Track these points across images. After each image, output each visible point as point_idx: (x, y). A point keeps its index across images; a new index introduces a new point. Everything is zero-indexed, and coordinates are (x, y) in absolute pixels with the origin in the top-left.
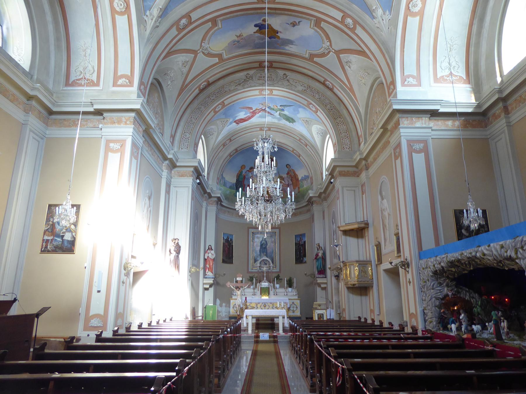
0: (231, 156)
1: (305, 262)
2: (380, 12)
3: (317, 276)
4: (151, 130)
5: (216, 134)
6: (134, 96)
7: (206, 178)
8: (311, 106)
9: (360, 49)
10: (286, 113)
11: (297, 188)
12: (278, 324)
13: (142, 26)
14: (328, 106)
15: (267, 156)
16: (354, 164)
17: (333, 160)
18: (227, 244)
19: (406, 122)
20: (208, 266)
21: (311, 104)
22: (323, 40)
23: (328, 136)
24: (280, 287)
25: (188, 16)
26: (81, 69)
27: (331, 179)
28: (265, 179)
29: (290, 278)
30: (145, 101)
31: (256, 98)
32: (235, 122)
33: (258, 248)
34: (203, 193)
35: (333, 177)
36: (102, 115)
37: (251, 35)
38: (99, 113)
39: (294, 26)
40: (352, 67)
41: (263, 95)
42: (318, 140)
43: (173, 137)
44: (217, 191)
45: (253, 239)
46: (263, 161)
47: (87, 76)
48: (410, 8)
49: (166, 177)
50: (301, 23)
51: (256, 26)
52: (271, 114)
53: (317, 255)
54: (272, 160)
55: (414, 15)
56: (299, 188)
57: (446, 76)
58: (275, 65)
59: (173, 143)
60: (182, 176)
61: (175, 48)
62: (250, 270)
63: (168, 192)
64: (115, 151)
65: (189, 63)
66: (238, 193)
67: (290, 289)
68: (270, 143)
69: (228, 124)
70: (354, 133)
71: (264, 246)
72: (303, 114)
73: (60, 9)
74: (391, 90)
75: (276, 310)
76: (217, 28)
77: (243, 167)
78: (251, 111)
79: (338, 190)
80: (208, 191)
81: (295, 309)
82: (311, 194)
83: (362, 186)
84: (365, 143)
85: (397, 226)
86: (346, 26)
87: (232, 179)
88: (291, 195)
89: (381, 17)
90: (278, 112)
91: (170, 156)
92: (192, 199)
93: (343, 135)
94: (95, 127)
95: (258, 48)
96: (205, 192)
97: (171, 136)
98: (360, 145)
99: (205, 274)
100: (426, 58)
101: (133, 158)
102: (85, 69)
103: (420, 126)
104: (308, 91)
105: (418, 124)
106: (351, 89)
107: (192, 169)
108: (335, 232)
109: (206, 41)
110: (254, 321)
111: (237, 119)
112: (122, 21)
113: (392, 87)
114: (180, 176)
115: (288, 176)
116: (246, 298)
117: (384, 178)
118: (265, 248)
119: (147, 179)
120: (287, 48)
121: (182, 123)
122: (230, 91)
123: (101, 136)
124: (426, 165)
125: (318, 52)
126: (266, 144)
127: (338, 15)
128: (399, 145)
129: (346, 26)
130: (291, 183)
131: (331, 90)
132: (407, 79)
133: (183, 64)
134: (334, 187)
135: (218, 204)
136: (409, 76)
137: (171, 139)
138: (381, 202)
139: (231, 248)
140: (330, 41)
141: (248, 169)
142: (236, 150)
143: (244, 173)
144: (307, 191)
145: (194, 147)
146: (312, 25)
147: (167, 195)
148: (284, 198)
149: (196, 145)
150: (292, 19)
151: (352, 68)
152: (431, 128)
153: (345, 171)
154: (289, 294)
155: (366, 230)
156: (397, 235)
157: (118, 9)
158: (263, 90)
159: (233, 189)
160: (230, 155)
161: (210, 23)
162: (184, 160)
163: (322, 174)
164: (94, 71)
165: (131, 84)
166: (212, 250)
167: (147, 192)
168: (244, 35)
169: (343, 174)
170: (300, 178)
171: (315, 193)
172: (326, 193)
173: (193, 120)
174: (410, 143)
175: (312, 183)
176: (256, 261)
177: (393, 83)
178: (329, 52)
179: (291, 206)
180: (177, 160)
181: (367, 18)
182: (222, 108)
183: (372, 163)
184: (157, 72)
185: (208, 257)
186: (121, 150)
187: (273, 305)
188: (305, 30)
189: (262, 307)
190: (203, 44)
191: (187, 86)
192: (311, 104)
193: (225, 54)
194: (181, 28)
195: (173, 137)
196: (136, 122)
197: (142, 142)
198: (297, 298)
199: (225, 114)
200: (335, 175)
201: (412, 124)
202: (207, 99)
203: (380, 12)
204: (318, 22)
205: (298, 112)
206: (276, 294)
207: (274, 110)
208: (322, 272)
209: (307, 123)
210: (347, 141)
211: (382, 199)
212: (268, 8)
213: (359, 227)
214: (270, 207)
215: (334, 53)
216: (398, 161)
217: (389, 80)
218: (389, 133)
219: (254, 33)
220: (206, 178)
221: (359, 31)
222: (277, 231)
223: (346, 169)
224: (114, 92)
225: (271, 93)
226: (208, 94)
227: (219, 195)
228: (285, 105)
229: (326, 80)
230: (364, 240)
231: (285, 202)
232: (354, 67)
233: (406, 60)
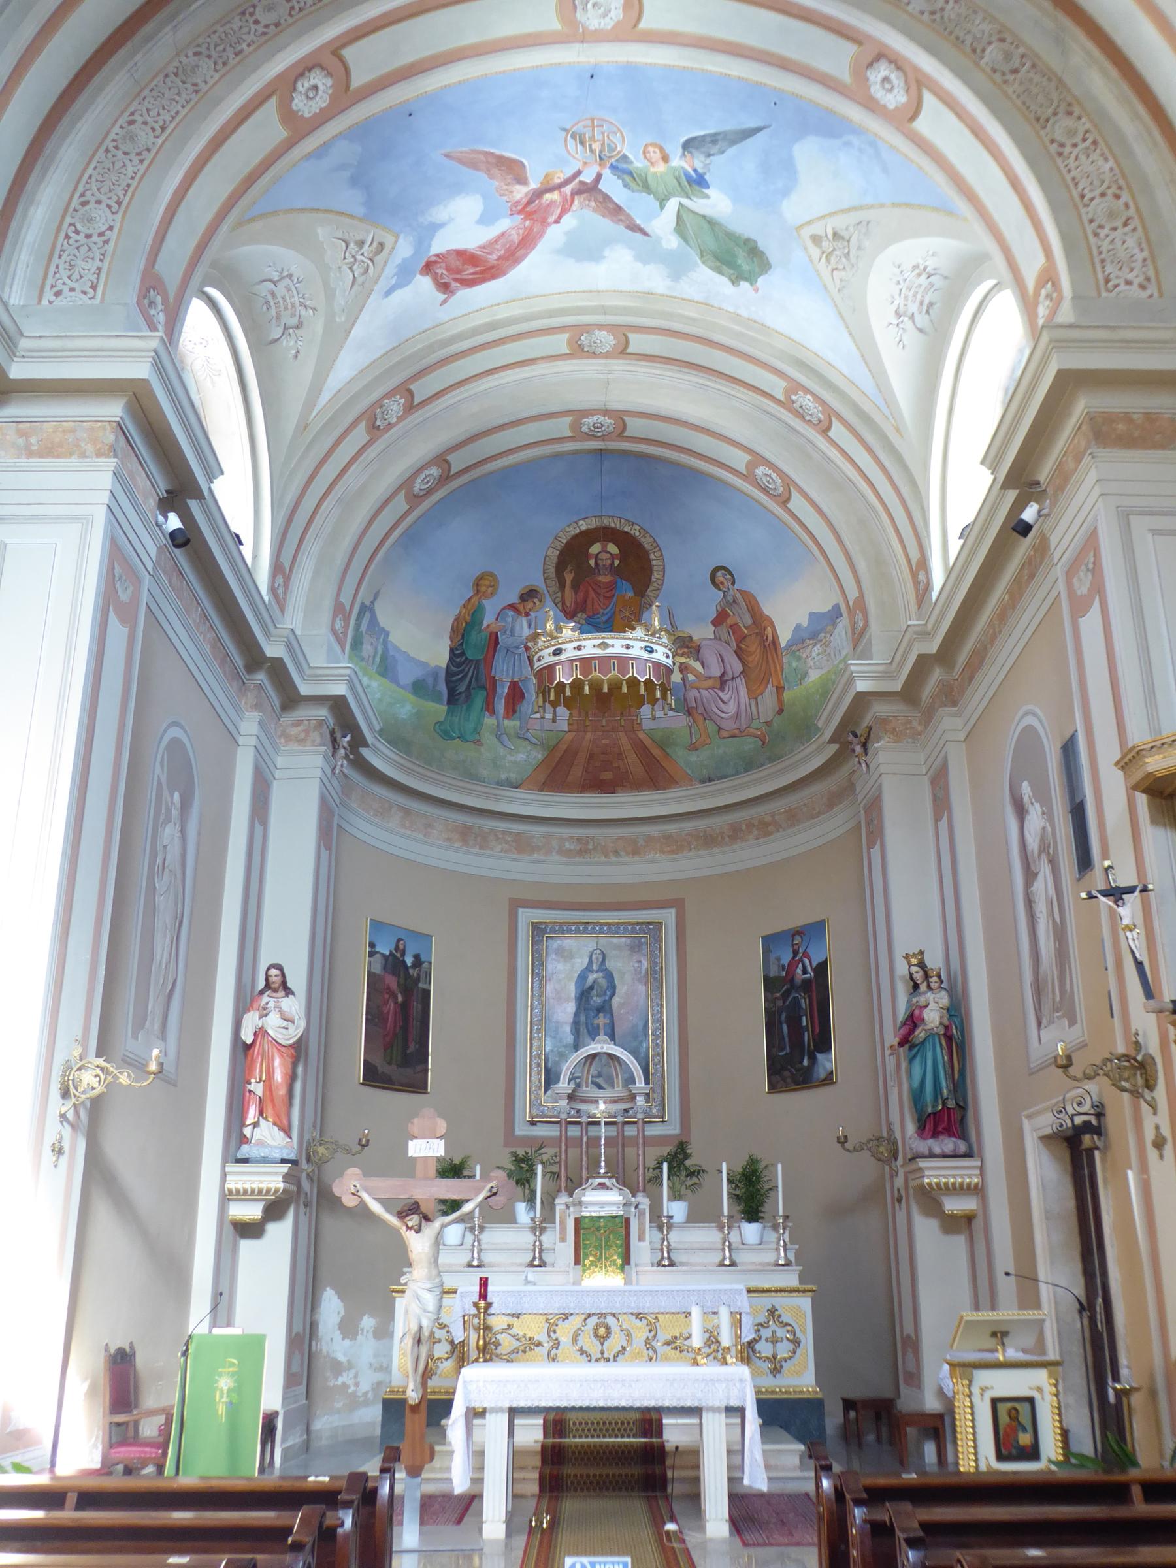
0: (415, 499)
1: (828, 1080)
3: (923, 1146)
5: (317, 326)
10: (716, 203)
11: (769, 693)
12: (693, 1457)
14: (993, 53)
18: (392, 981)
20: (257, 1088)
21: (882, 55)
24: (694, 1218)
27: (1019, 505)
29: (753, 1161)
32: (428, 267)
33: (566, 1011)
34: (239, 662)
45: (539, 962)
52: (635, 228)
53: (913, 1021)
56: (780, 690)
60: (49, 450)
67: (751, 1231)
71: (596, 1000)
75: (683, 1370)
77: (484, 584)
78: (520, 192)
79: (1091, 542)
80: (272, 650)
81: (783, 1350)
93: (1099, 207)
96: (254, 659)
99: (235, 1135)
107: (115, 409)
110: (531, 1434)
114: (31, 454)
115: (723, 631)
116: (484, 1283)
118: (605, 1008)
130: (737, 667)
134: (1043, 548)
139: (416, 1006)
141: (514, 599)
143: (488, 619)
153: (1127, 418)
154: (742, 1257)
159: (436, 698)
166: (289, 992)
169: (1107, 433)
170: (784, 637)
173: (144, 137)
176: (551, 1077)
185: (260, 1033)
187: (652, 1329)
189: (588, 1342)
198: (791, 1279)
202: (236, 23)
206: (667, 1261)
207: (646, 187)
208: (947, 1118)
227: (340, 690)
228: (714, 139)
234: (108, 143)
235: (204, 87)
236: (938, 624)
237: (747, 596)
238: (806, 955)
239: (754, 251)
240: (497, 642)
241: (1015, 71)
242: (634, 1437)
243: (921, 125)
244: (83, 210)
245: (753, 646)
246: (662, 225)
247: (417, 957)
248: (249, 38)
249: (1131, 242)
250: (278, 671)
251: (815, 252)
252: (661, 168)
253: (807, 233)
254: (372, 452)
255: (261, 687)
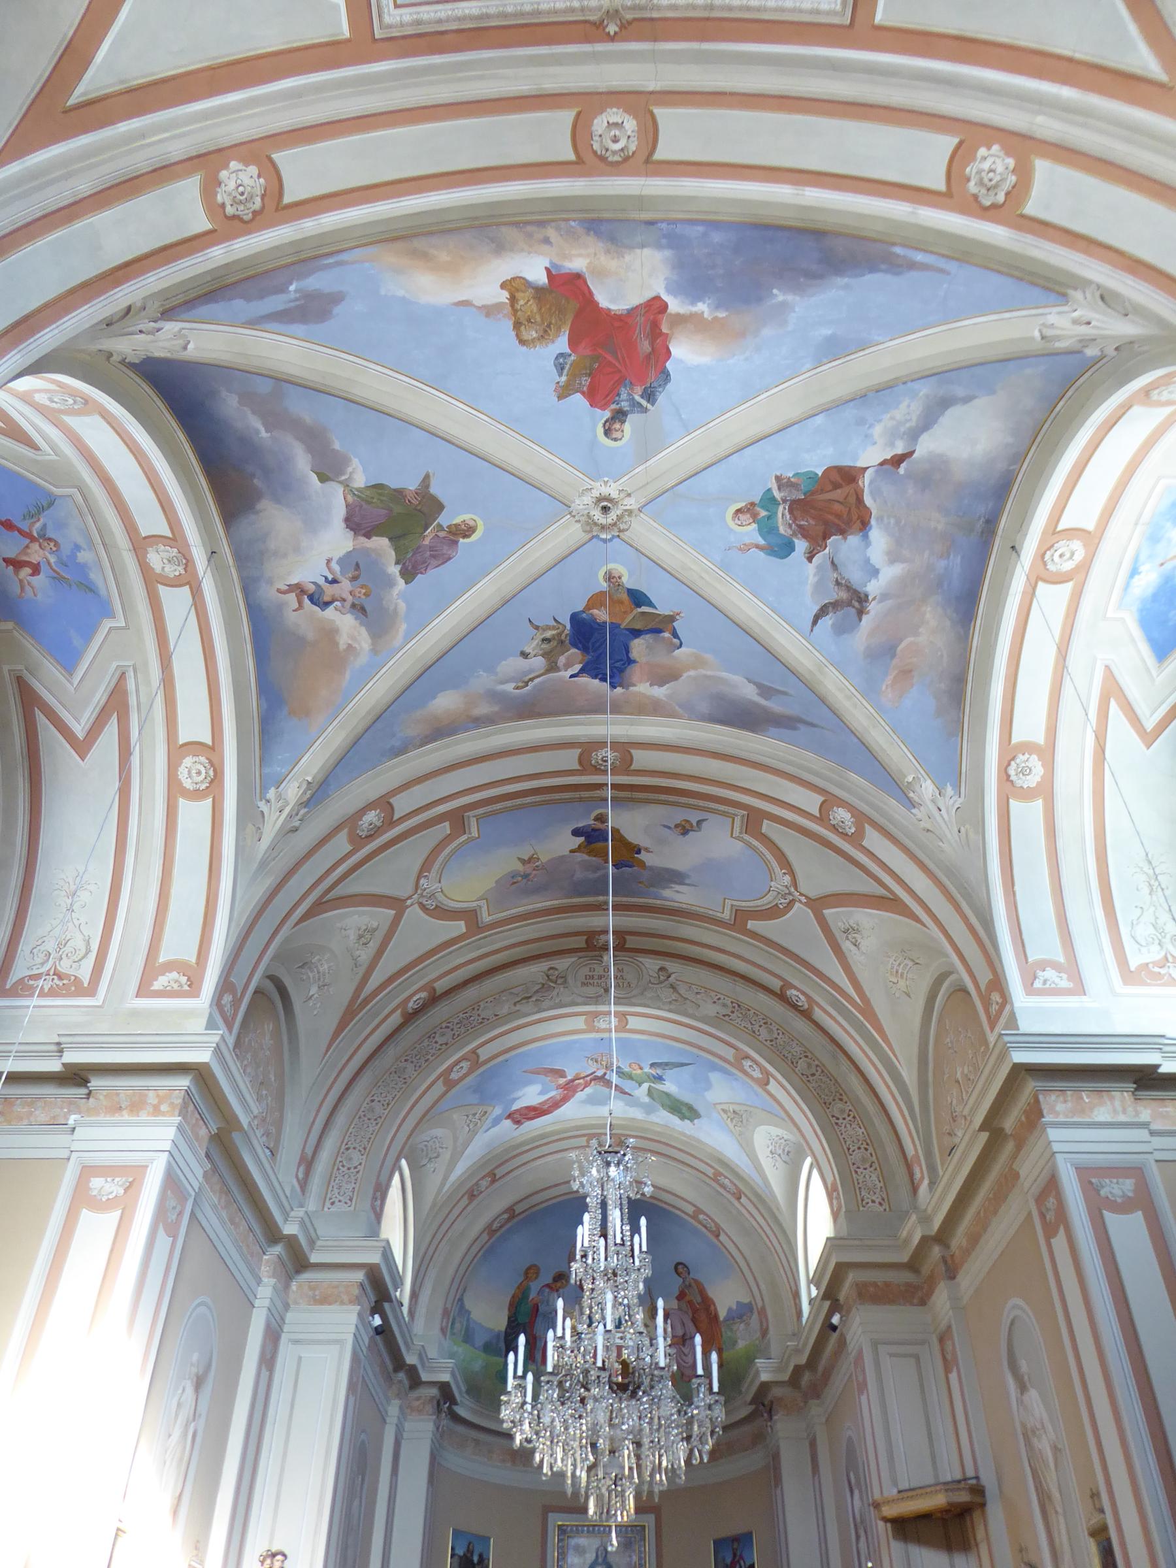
2: (927, 788)
4: (236, 1137)
5: (446, 1156)
6: (198, 1024)
7: (405, 1310)
8: (747, 1064)
9: (881, 891)
13: (250, 828)
14: (802, 1064)
15: (617, 1213)
16: (905, 1258)
17: (832, 1245)
19: (1060, 1107)
21: (747, 1057)
22: (771, 871)
23: (808, 1161)
25: (384, 803)
26: (50, 946)
27: (830, 1314)
28: (608, 1310)
30: (231, 1041)
31: (575, 1042)
32: (509, 1116)
34: (390, 1367)
35: (835, 1307)
36: (84, 1082)
37: (563, 857)
38: (76, 1077)
39: (685, 832)
40: (864, 944)
41: (599, 1031)
42: (774, 1175)
43: (308, 1163)
44: (437, 1356)
45: (562, 1555)
46: (604, 1235)
47: (64, 967)
48: (1013, 778)
49: (267, 1303)
50: (704, 824)
51: (576, 833)
54: (635, 1230)
55: (1027, 795)
57: (1155, 963)
58: (632, 942)
59: (304, 1184)
60: (324, 1300)
61: (339, 891)
62: (377, 37)
63: (268, 1361)
64: (100, 1205)
65: (379, 936)
66: (511, 1356)
68: (626, 1168)
69: (489, 1122)
70: (891, 1149)
72: (722, 1091)
73: (27, 785)
74: (995, 1007)
76: (464, 838)
77: (531, 1272)
78: (562, 1081)
79: (860, 1352)
80: (411, 1359)
82: (765, 1371)
83: (941, 1340)
84: (932, 1184)
85: (1095, 1495)
86: (835, 829)
87: (491, 1316)
88: (706, 1363)
89: (933, 801)
90: (646, 1086)
91: (290, 1229)
92: (352, 1387)
93: (857, 1156)
94: (56, 1124)
95: (581, 895)
97: (303, 1159)
98: (915, 1190)
100: (1085, 913)
101: (161, 1232)
102: (62, 945)
103: (1109, 1119)
104: (733, 1017)
105: (1102, 1114)
106: (868, 1010)
107: (360, 1276)
108: (861, 1526)
109: (433, 874)
111: (515, 1107)
112: (194, 816)
113: (996, 997)
117: (1016, 1305)
119: (203, 1309)
120: (667, 893)
121: (341, 1119)
122: (499, 1019)
123: (65, 1154)
124: (1158, 1256)
125: (759, 902)
126: (613, 1171)
127: (811, 802)
128: (1052, 1184)
129: (835, 829)
131: (806, 1014)
132: (1040, 973)
133: (361, 937)
134: (842, 1343)
135: (439, 1410)
136: (1043, 965)
137: (302, 1169)
138: (1020, 1402)
140: (792, 873)
141: (549, 1281)
142: (510, 1210)
144: (750, 1360)
145: (374, 1199)
146: (736, 833)
147: (265, 1373)
148: (683, 1380)
149: (381, 1192)
150: (680, 815)
151: (863, 948)
152: (1144, 1125)
153: (875, 1284)
155: (977, 1515)
156: (1100, 1533)
157: (188, 784)
158: (596, 1015)
160: (490, 1230)
161: (447, 824)
162: (339, 1244)
163: (796, 1295)
164: (88, 951)
165: (193, 989)
167: (195, 1357)
168: (544, 858)
170: (722, 1314)
171: (779, 1369)
172: (818, 1370)
174: (1089, 1175)
175: (764, 1332)
177: (998, 984)
178: (792, 902)
179: (708, 1409)
180: (312, 1243)
181: (893, 806)
182: (471, 1071)
183: (967, 1252)
184: (275, 958)
186: (126, 1205)
188: (719, 841)
190: (422, 881)
191: (366, 1001)
192: (747, 1057)
193: (485, 908)
194: (364, 834)
195: (308, 1163)
196: (191, 1107)
197: (200, 1173)
199: (478, 1089)
200: (842, 1297)
201: (1083, 1112)
203: (927, 788)
204: (753, 821)
205: (708, 1086)
209: (738, 1118)
210: (873, 1178)
211: (1023, 1388)
212: (614, 786)
213: (951, 1504)
214: (630, 1414)
215: (805, 904)
216: (1059, 1242)
217: (984, 977)
218: (1010, 1146)
219: (572, 851)
220: (405, 1310)
221: (873, 840)
222: (649, 1520)
223: (879, 1277)
224: (135, 1013)
225: (622, 1027)
226: (430, 1029)
227: (445, 1377)
228: (667, 1064)
229: (787, 985)
230: (973, 1559)
231: (686, 1396)
232: (869, 942)
233: (1027, 925)
234: (360, 1113)
235: (409, 1081)
236: (805, 1344)
237: (696, 1281)
238: (741, 1557)
239: (691, 1108)
240: (537, 1310)
241: (813, 1075)
242: (607, 862)
243: (769, 1087)
244: (347, 1153)
245: (703, 1316)
246: (641, 1092)
247: (481, 1556)
248: (432, 1051)
249: (874, 1177)
250: (412, 1372)
251: (725, 1116)
252: (639, 1071)
253: (719, 1107)
254: (470, 1208)
255: (400, 1382)
